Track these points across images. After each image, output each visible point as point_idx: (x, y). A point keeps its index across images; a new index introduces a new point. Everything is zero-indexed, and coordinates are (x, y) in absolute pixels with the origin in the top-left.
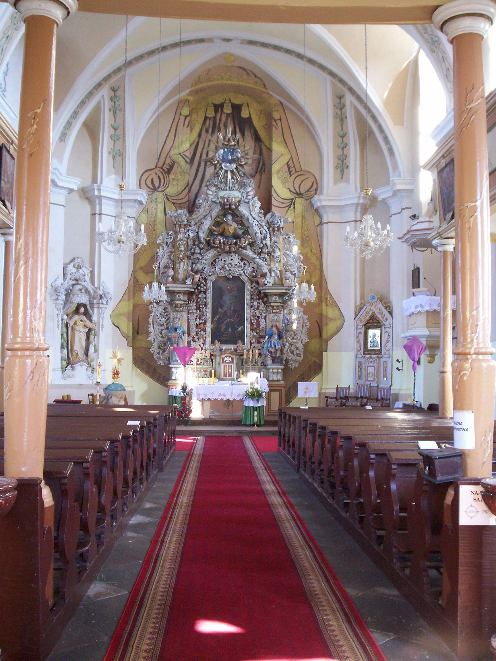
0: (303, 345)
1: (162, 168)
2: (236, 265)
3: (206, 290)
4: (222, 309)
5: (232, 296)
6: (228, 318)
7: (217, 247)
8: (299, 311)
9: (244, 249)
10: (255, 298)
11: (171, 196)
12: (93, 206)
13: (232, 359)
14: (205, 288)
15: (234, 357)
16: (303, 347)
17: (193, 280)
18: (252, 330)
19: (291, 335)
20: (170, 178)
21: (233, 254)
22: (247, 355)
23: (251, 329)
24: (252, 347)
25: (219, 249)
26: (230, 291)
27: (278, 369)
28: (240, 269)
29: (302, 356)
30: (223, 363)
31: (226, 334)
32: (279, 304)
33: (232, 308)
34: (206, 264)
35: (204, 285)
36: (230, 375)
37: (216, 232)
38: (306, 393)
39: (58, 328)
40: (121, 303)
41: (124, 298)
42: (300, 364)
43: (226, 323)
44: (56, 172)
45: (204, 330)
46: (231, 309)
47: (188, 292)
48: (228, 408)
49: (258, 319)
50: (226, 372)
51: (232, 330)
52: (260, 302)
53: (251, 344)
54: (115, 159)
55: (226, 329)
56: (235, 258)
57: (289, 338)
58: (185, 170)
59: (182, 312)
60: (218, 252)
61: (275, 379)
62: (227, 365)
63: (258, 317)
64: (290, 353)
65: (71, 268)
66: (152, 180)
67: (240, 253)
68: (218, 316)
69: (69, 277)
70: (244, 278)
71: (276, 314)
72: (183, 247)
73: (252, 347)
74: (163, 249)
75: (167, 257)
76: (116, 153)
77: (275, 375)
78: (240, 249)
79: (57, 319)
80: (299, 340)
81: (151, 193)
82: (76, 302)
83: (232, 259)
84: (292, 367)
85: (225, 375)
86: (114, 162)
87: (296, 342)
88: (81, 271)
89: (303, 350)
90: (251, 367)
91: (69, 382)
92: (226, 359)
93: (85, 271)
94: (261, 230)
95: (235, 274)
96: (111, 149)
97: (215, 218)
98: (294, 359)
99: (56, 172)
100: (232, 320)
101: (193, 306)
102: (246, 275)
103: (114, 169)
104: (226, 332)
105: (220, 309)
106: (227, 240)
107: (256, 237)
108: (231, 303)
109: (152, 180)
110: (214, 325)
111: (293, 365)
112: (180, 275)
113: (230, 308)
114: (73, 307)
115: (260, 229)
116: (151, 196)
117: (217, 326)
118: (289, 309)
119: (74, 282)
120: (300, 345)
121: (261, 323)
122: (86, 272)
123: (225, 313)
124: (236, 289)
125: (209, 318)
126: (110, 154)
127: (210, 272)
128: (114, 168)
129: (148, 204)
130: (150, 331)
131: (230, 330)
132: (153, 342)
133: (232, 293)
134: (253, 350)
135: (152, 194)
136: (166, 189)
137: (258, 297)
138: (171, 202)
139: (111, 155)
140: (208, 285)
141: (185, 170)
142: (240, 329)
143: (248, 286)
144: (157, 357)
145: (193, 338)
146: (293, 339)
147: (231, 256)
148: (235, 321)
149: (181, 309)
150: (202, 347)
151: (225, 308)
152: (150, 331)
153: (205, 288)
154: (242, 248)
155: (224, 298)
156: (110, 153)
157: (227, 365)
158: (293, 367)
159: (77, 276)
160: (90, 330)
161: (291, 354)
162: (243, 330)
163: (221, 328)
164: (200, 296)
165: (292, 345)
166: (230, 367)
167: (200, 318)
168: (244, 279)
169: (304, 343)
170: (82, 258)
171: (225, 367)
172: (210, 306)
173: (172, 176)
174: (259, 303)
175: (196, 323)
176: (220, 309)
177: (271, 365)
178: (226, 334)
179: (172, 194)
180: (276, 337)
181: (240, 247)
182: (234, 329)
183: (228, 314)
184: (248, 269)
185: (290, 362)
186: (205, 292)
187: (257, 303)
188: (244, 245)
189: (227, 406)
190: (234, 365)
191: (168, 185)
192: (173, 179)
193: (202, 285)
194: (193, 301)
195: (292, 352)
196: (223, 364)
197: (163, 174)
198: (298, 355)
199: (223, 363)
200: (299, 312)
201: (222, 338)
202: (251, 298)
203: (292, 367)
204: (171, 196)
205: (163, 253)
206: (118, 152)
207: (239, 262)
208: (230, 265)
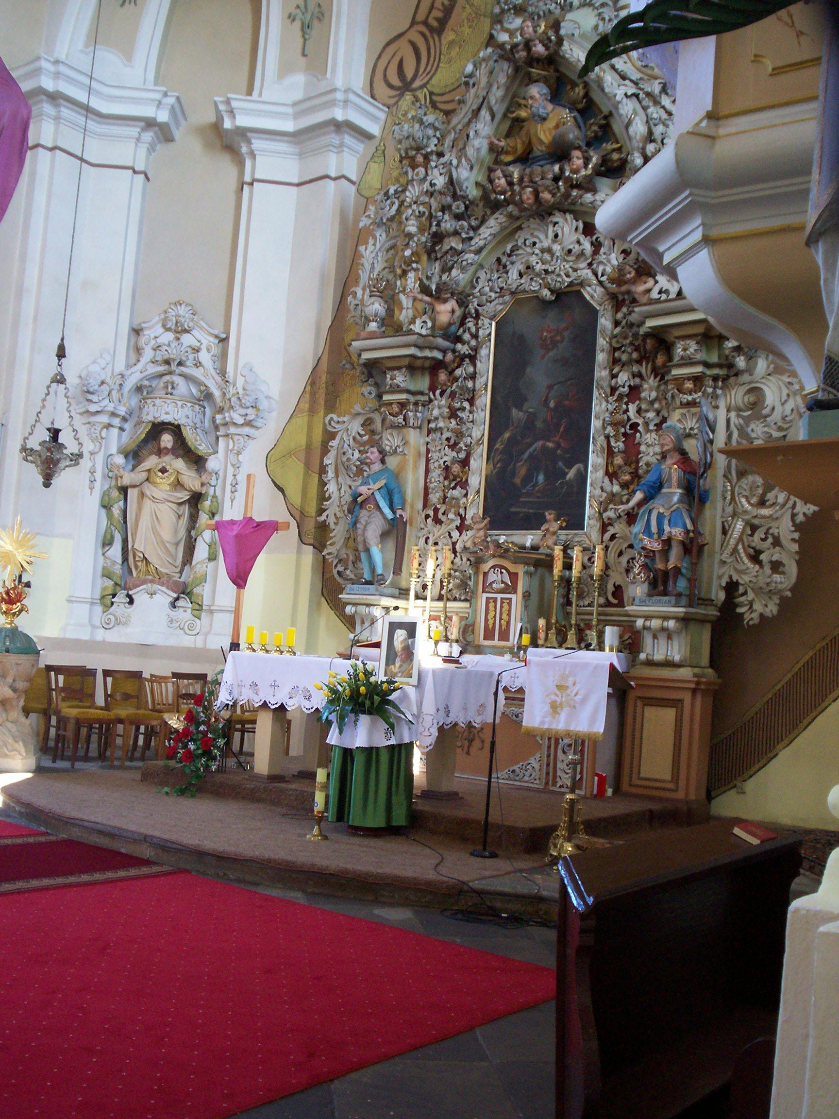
0: (798, 527)
1: (425, 23)
2: (570, 251)
3: (476, 349)
4: (520, 410)
5: (556, 361)
6: (536, 440)
7: (507, 202)
8: (785, 391)
9: (588, 190)
10: (624, 357)
11: (442, 95)
12: (241, 164)
13: (514, 576)
14: (473, 343)
15: (520, 570)
16: (796, 536)
17: (434, 321)
18: (612, 475)
19: (753, 487)
20: (444, 42)
21: (558, 217)
22: (584, 567)
23: (607, 473)
24: (607, 536)
25: (510, 208)
26: (548, 345)
27: (666, 618)
28: (583, 265)
29: (792, 569)
30: (483, 592)
31: (529, 494)
32: (699, 369)
33: (552, 404)
34: (481, 266)
35: (471, 334)
36: (504, 635)
37: (507, 153)
38: (555, 708)
39: (92, 488)
40: (294, 420)
41: (301, 405)
42: (784, 603)
43: (531, 455)
44: (62, 68)
45: (464, 484)
46: (548, 407)
47: (427, 364)
48: (468, 753)
49: (634, 435)
50: (491, 622)
51: (547, 479)
52: (643, 371)
53: (604, 528)
54: (308, 31)
55: (528, 478)
56: (566, 229)
57: (743, 500)
58: (482, 8)
59: (405, 430)
60: (510, 216)
61: (659, 657)
62: (495, 600)
63: (634, 426)
64: (745, 560)
65: (155, 333)
66: (401, 63)
67: (578, 208)
68: (507, 435)
69: (148, 354)
70: (593, 294)
71: (693, 410)
72: (412, 222)
73: (607, 536)
74: (374, 245)
75: (385, 265)
76: (313, 14)
77: (662, 641)
78: (574, 193)
79: (90, 464)
80: (783, 505)
81: (395, 99)
82: (150, 418)
83: (556, 236)
84: (752, 617)
85: (489, 635)
86: (305, 40)
87: (770, 516)
88: (187, 339)
89: (795, 547)
90: (594, 609)
91: (113, 636)
92: (492, 577)
93: (199, 337)
94: (650, 111)
95: (563, 281)
96: (298, 7)
97: (508, 110)
98: (762, 581)
99: (62, 68)
100: (550, 445)
101: (440, 406)
102: (601, 283)
103: (304, 59)
104: (528, 488)
105: (514, 412)
106: (528, 171)
107: (630, 138)
108: (550, 387)
109: (401, 63)
110: (495, 467)
111: (757, 606)
112: (404, 311)
113: (546, 401)
114: (141, 433)
115: (645, 109)
116: (394, 109)
117: (503, 470)
118: (747, 387)
119: (162, 368)
120: (785, 529)
121: (643, 448)
122: (205, 343)
123: (529, 425)
124: (566, 334)
125: (479, 442)
126: (293, 20)
127: (491, 290)
128: (304, 55)
129: (384, 136)
130: (327, 496)
131: (541, 478)
132: (332, 526)
133: (555, 351)
134: (607, 547)
135: (396, 103)
136: (431, 79)
137: (635, 355)
138: (441, 111)
139: (297, 24)
140: (481, 332)
141: (482, 8)
142: (571, 474)
143: (605, 322)
144: (339, 573)
145: (436, 510)
146: (762, 503)
147: (555, 224)
148: (558, 445)
149: (400, 419)
150: (454, 540)
151: (531, 406)
152: (327, 496)
153: (473, 343)
154: (578, 186)
155: (529, 370)
156: (292, 18)
157: (495, 600)
158: (755, 615)
159: (174, 352)
160: (196, 499)
161: (750, 565)
162: (582, 478)
163: (513, 474)
164: (458, 372)
165: (754, 528)
166: (491, 605)
167: (453, 447)
168: (592, 297)
169: (800, 518)
170: (190, 305)
171: (491, 605)
172: (485, 400)
173: (449, 36)
174: (640, 375)
175: (442, 462)
176: (514, 412)
177: (643, 603)
178: (529, 494)
179: (446, 86)
180: (675, 493)
181: (573, 187)
182: (554, 475)
183: (539, 424)
184: (609, 261)
185: (745, 593)
186: (473, 359)
187: (634, 376)
188: (583, 173)
189: (466, 743)
190: (516, 599)
191: (438, 66)
192: (451, 43)
193: (467, 337)
194: (442, 394)
195: (755, 557)
196: (485, 595)
197: (426, 40)
198: (776, 566)
199: (483, 592)
200: (784, 397)
201: (513, 510)
202: (615, 361)
203: (752, 617)
204: (442, 95)
205: (373, 255)
206: (317, 10)
207: (578, 242)
208: (547, 256)
